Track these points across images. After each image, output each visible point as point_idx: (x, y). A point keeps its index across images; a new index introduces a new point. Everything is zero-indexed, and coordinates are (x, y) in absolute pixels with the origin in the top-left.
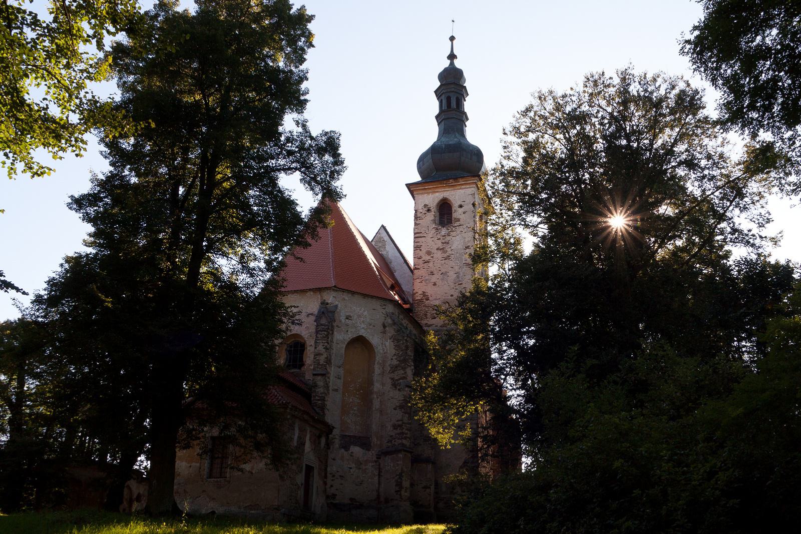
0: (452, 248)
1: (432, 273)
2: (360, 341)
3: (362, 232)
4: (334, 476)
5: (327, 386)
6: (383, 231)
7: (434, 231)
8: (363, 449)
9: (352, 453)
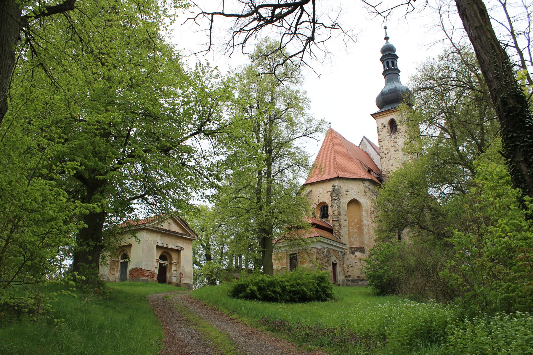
2: (354, 202)
5: (340, 226)
6: (365, 140)
7: (388, 137)
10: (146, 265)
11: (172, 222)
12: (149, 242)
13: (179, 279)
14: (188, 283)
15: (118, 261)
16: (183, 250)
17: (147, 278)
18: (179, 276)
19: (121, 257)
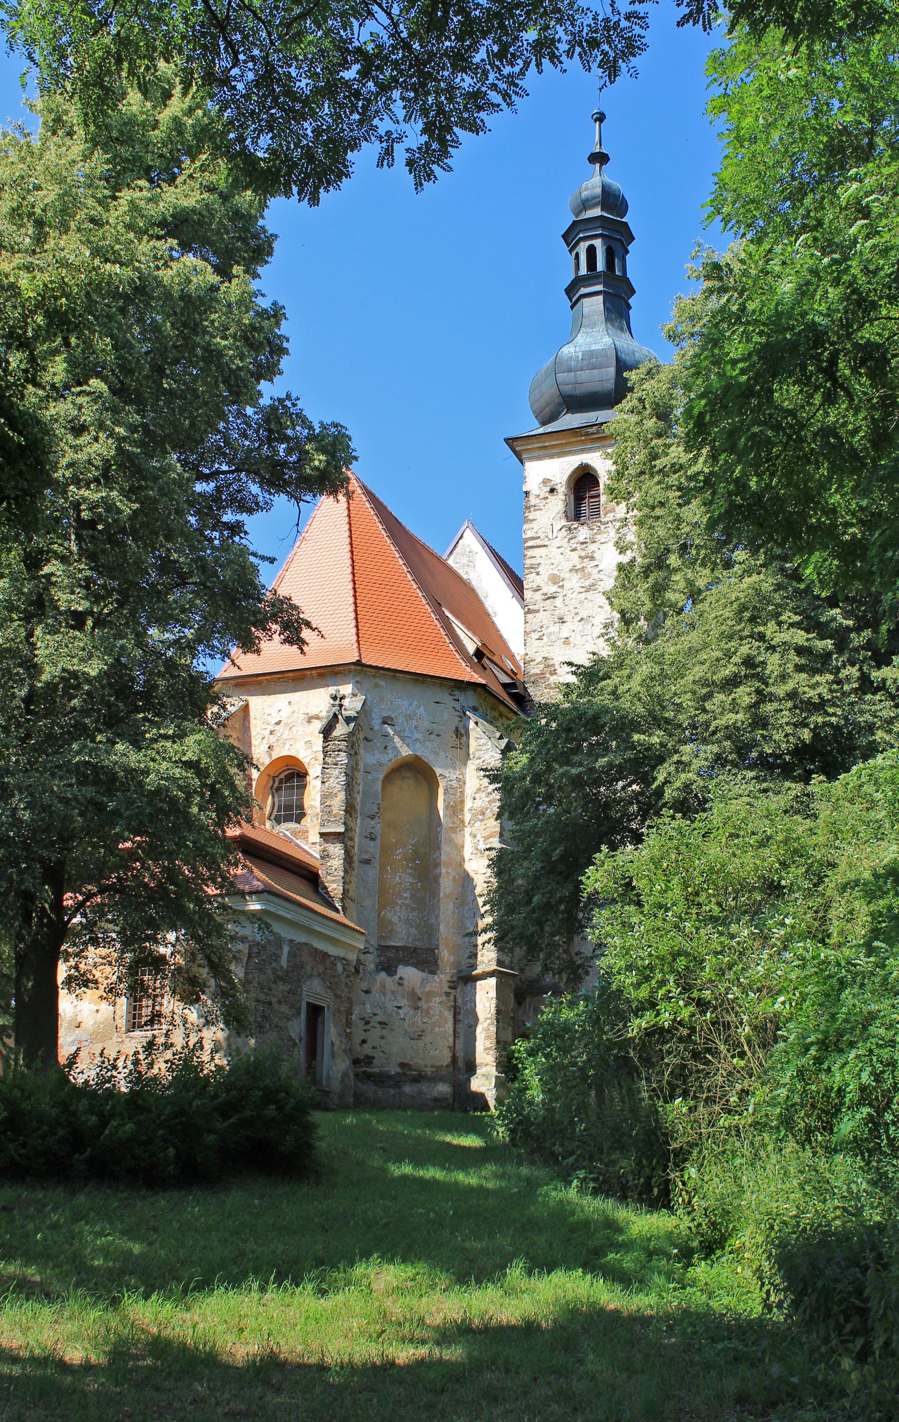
0: (600, 568)
1: (562, 620)
4: (367, 1023)
7: (564, 532)
8: (423, 971)
9: (401, 978)
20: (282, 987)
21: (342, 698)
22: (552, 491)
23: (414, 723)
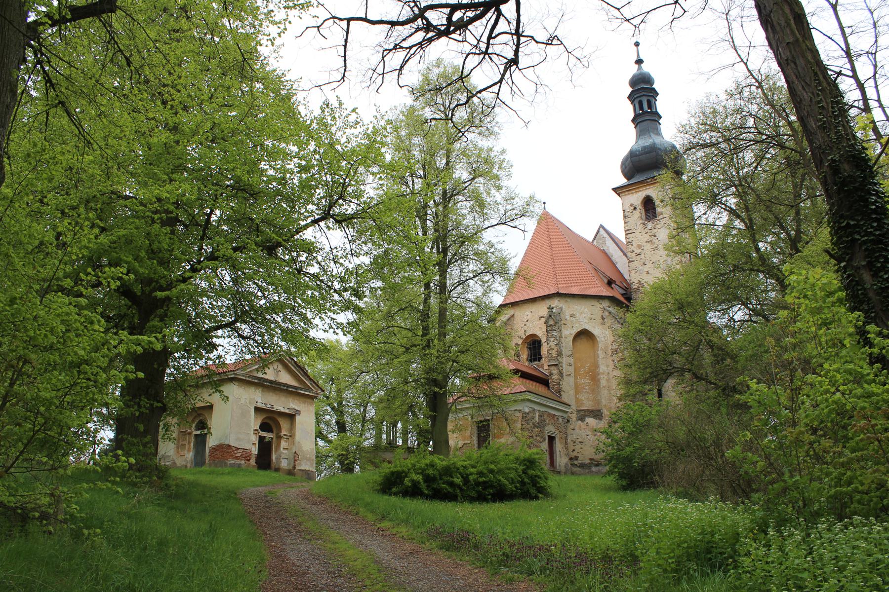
2: (584, 334)
3: (834, 16)
5: (561, 374)
7: (642, 226)
10: (238, 439)
11: (280, 367)
12: (243, 401)
13: (292, 462)
14: (307, 469)
15: (190, 434)
16: (299, 414)
17: (238, 462)
18: (292, 457)
19: (196, 426)
20: (537, 430)
21: (553, 308)
22: (635, 209)
23: (584, 315)
